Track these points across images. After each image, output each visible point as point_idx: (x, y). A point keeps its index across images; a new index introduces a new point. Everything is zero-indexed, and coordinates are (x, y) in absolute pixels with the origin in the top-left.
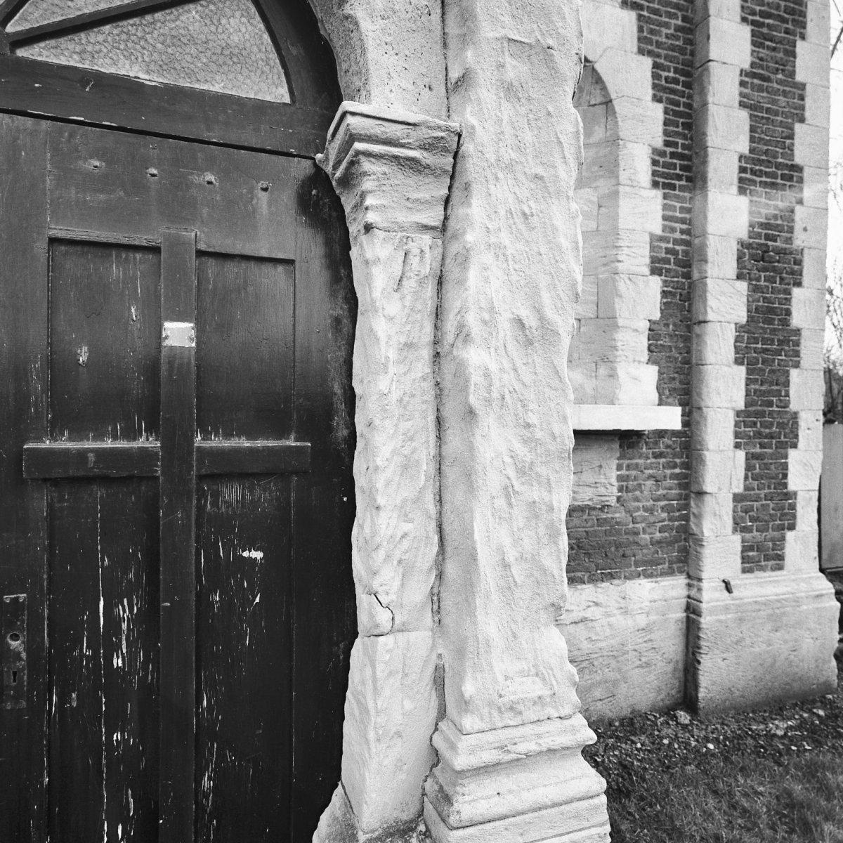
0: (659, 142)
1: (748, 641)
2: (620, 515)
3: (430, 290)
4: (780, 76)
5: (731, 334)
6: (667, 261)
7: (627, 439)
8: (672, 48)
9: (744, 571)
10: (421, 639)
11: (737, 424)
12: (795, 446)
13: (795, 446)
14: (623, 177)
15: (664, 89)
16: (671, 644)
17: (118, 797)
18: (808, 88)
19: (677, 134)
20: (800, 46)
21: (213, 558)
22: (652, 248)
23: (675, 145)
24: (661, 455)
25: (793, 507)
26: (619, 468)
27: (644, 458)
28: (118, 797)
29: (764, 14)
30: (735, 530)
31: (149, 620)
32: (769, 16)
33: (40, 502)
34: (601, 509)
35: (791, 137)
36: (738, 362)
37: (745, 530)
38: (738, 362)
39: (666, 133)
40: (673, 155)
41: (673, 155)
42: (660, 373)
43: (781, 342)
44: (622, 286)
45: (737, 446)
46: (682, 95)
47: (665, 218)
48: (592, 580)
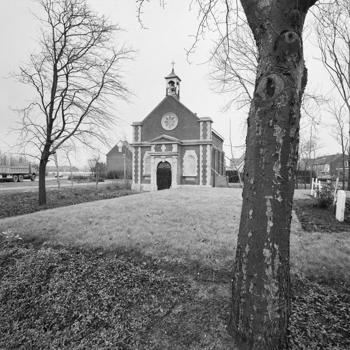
7: (195, 177)
27: (197, 178)
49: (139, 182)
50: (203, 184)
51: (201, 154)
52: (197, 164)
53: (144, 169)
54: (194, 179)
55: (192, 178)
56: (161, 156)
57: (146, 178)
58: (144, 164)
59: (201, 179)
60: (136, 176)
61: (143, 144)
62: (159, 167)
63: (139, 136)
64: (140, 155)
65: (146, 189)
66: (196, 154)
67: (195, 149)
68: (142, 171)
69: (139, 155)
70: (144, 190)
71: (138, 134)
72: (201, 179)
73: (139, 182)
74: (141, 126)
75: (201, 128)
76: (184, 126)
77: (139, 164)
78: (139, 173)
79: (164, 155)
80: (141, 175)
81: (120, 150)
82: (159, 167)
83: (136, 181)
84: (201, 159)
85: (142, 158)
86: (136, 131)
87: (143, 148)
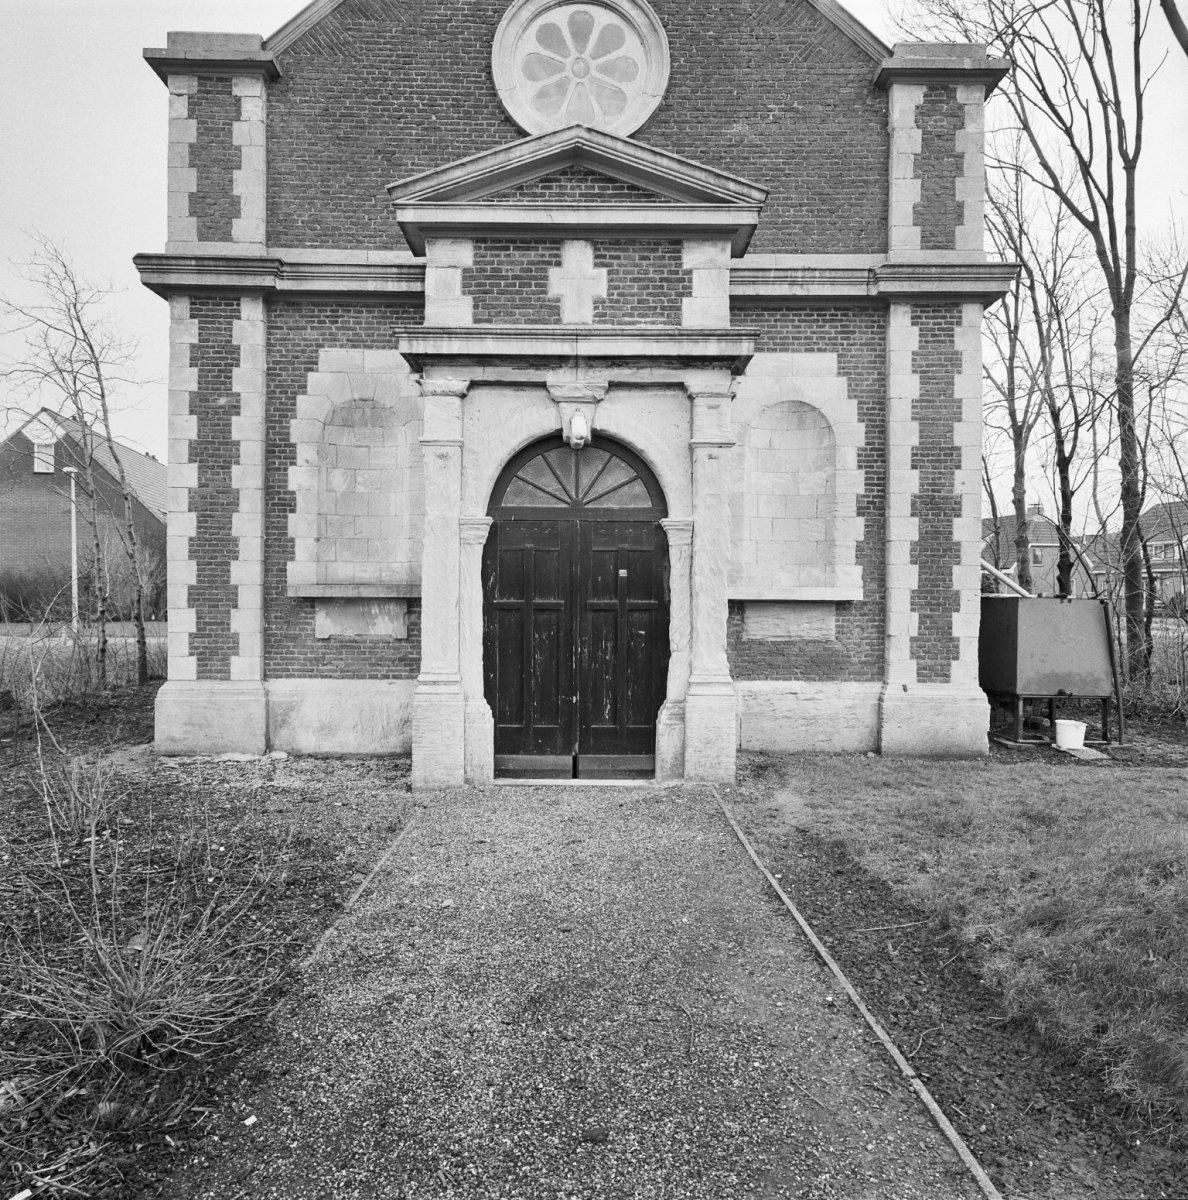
0: (862, 444)
1: (916, 719)
2: (838, 646)
3: (688, 560)
4: (942, 398)
5: (907, 547)
6: (869, 508)
7: (842, 606)
8: (871, 391)
9: (919, 681)
10: (686, 654)
11: (912, 598)
12: (958, 610)
13: (958, 610)
14: (838, 466)
15: (865, 414)
16: (870, 719)
17: (607, 694)
18: (964, 401)
19: (873, 438)
20: (957, 378)
21: (631, 634)
22: (858, 502)
23: (874, 444)
24: (864, 615)
25: (957, 647)
26: (837, 621)
27: (853, 617)
28: (607, 694)
29: (927, 366)
30: (912, 658)
31: (615, 648)
32: (933, 366)
33: (590, 615)
34: (826, 642)
35: (951, 431)
36: (913, 562)
37: (918, 657)
38: (913, 562)
39: (866, 438)
40: (872, 450)
41: (872, 450)
42: (864, 570)
43: (944, 550)
44: (838, 524)
45: (913, 610)
46: (878, 415)
47: (866, 485)
48: (820, 680)
49: (247, 662)
50: (925, 675)
51: (904, 386)
52: (853, 483)
53: (298, 525)
54: (821, 628)
55: (815, 614)
56: (549, 376)
57: (325, 624)
58: (297, 478)
59: (903, 622)
60: (213, 595)
61: (298, 270)
62: (510, 501)
63: (250, 184)
64: (260, 380)
65: (326, 729)
66: (852, 394)
67: (832, 346)
68: (277, 547)
69: (249, 380)
70: (308, 742)
71: (231, 161)
72: (903, 622)
73: (247, 662)
74: (271, 76)
75: (907, 140)
76: (731, 120)
77: (247, 476)
78: (247, 573)
79: (593, 361)
80: (266, 588)
81: (43, 464)
82: (510, 501)
83: (213, 653)
84: (904, 436)
85: (278, 412)
86: (204, 130)
87: (292, 319)
